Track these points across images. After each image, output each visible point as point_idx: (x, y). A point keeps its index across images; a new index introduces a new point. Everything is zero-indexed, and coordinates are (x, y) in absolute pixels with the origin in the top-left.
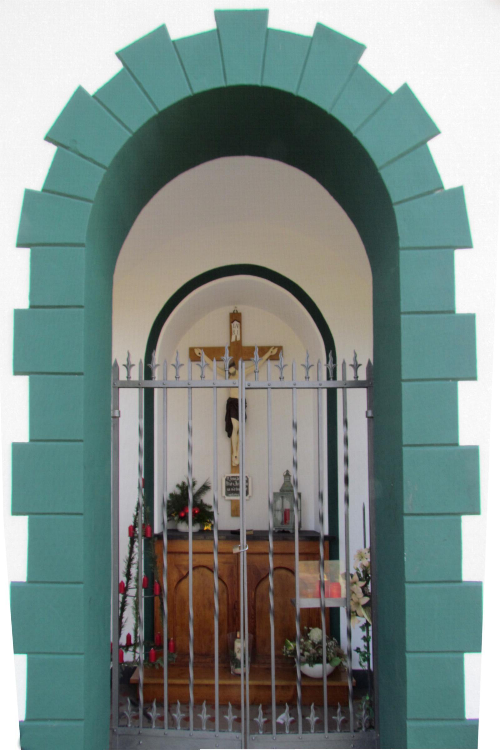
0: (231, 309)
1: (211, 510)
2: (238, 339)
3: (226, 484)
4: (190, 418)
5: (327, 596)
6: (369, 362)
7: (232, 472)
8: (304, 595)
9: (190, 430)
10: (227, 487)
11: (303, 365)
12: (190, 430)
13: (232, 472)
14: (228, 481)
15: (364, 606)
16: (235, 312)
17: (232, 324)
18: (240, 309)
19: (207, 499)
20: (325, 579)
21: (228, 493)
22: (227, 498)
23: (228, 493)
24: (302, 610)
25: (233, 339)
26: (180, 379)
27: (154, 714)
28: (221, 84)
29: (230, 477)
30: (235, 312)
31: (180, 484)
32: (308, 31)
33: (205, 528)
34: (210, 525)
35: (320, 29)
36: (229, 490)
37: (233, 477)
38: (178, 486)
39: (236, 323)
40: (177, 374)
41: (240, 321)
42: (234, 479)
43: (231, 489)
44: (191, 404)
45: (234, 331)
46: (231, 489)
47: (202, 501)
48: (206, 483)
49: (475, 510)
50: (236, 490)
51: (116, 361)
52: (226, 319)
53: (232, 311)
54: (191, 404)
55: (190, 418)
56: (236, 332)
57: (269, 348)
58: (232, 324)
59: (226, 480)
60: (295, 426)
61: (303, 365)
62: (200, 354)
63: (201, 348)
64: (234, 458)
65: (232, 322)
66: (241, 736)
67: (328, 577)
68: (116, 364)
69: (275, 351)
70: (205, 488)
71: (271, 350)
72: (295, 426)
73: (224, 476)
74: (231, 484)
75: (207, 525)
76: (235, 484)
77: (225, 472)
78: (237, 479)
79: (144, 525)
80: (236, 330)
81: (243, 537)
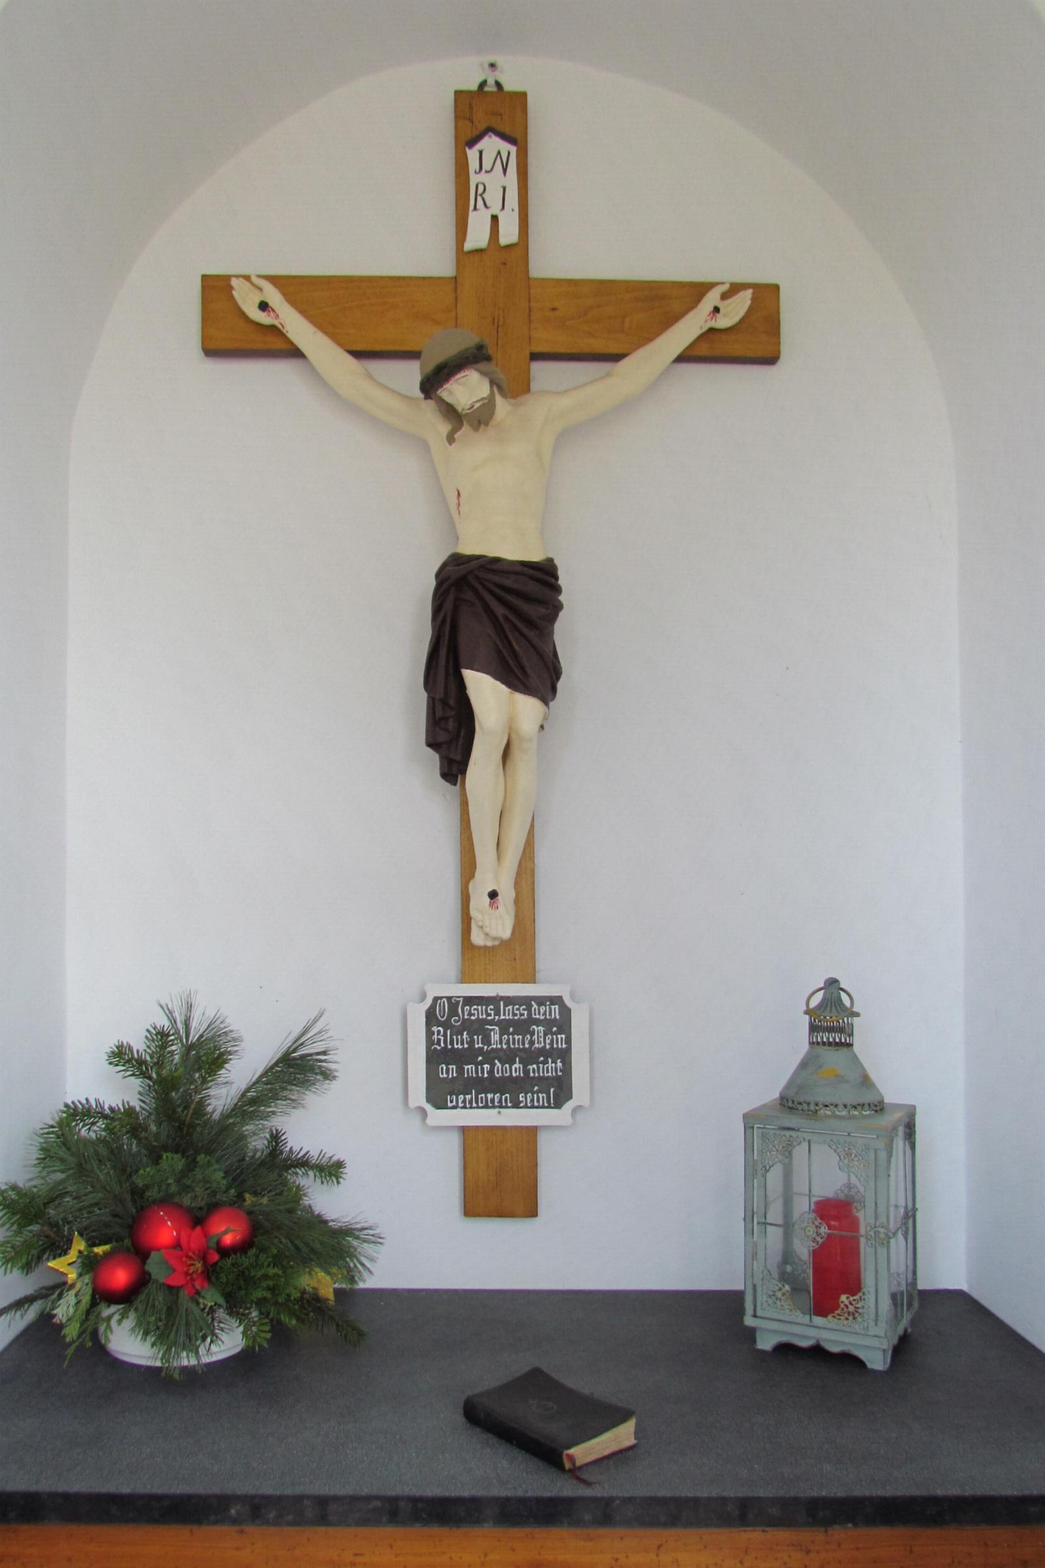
2: (509, 233)
3: (430, 1042)
7: (466, 977)
10: (435, 1058)
13: (466, 977)
14: (446, 1025)
16: (490, 88)
17: (472, 154)
21: (439, 1094)
22: (438, 1117)
23: (439, 1094)
25: (477, 237)
29: (453, 1003)
30: (490, 88)
31: (139, 1044)
36: (448, 1071)
37: (469, 1001)
38: (121, 1056)
39: (491, 145)
41: (517, 138)
42: (478, 1013)
43: (460, 1070)
44: (810, 1186)
45: (481, 193)
46: (460, 1070)
47: (276, 1137)
48: (298, 1043)
50: (491, 1072)
54: (810, 1186)
56: (493, 197)
57: (698, 291)
58: (472, 154)
59: (431, 1017)
62: (264, 306)
64: (480, 901)
65: (467, 139)
69: (735, 311)
71: (712, 299)
73: (423, 997)
74: (460, 1043)
76: (487, 1040)
78: (497, 1013)
79: (237, 1174)
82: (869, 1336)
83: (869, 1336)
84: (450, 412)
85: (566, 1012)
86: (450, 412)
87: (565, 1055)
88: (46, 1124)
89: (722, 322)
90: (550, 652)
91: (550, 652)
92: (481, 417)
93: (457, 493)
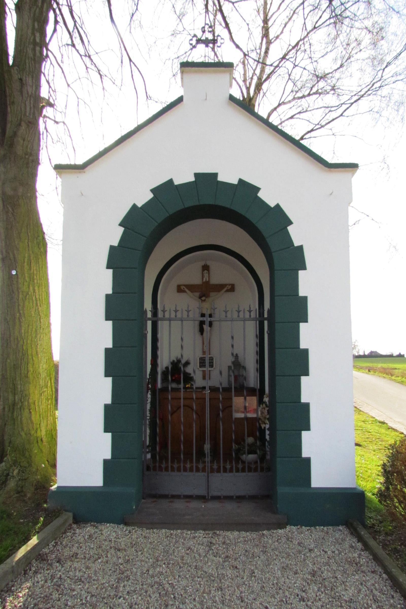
0: (203, 263)
1: (191, 376)
2: (207, 280)
4: (182, 334)
5: (248, 412)
6: (268, 309)
8: (237, 411)
9: (182, 339)
10: (200, 363)
11: (236, 311)
12: (182, 339)
13: (203, 355)
15: (268, 419)
17: (204, 272)
18: (208, 263)
19: (189, 369)
20: (247, 405)
21: (201, 366)
23: (201, 366)
24: (236, 419)
25: (204, 280)
26: (177, 317)
27: (163, 466)
28: (197, 203)
29: (202, 357)
32: (235, 182)
33: (187, 386)
34: (190, 384)
35: (241, 181)
36: (201, 364)
39: (206, 271)
40: (176, 315)
44: (182, 328)
49: (307, 374)
51: (146, 309)
52: (200, 269)
53: (203, 264)
54: (182, 328)
55: (182, 334)
59: (200, 359)
60: (232, 338)
61: (236, 311)
62: (184, 289)
63: (184, 285)
65: (203, 270)
66: (206, 474)
67: (248, 404)
68: (146, 310)
69: (230, 287)
70: (187, 363)
71: (227, 286)
72: (232, 338)
75: (188, 384)
77: (199, 354)
80: (206, 275)
81: (207, 388)
82: (97, 68)
83: (97, 68)
84: (202, 300)
85: (213, 358)
86: (202, 300)
87: (213, 363)
88: (305, 139)
89: (228, 289)
90: (267, 446)
91: (267, 446)
92: (205, 300)
93: (331, 193)
